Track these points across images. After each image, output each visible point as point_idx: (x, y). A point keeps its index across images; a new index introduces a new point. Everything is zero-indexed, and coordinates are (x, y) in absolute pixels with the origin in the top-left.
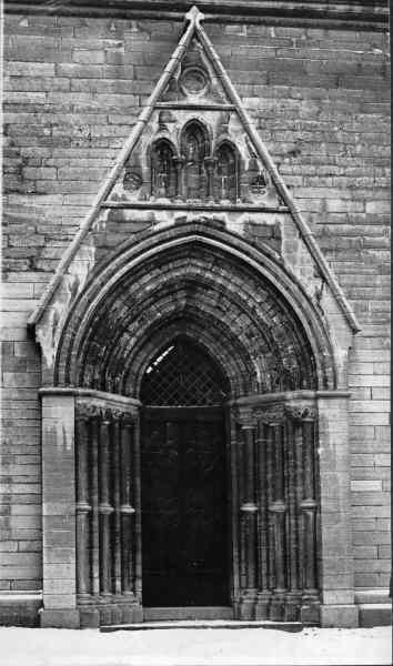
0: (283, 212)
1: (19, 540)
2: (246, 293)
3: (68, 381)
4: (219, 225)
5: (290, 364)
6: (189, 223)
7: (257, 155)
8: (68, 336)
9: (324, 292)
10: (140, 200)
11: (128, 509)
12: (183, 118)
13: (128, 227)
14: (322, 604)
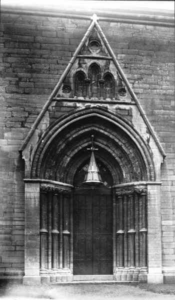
7: (122, 79)
8: (37, 156)
9: (151, 139)
10: (70, 97)
11: (66, 232)
12: (89, 62)
13: (64, 109)
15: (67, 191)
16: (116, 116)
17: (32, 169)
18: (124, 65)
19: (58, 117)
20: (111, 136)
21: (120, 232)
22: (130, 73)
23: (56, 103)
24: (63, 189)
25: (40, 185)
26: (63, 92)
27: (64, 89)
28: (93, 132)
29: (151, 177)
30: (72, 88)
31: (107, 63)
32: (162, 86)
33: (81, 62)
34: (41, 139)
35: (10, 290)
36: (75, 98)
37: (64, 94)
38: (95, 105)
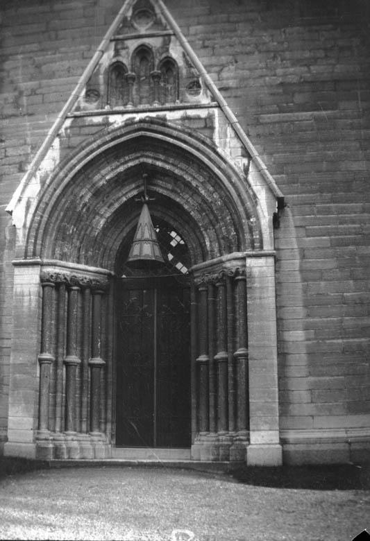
0: (215, 107)
1: (40, 392)
2: (191, 175)
3: (34, 255)
4: (162, 122)
5: (228, 232)
6: (136, 123)
7: (190, 64)
8: (37, 218)
9: (251, 169)
10: (98, 109)
11: (98, 360)
12: (133, 45)
13: (86, 130)
14: (249, 444)
15: (97, 281)
16: (183, 131)
17: (27, 242)
18: (201, 42)
19: (75, 145)
20: (177, 171)
21: (203, 358)
22: (213, 55)
23: (72, 122)
24: (87, 277)
25: (41, 271)
26: (86, 101)
27: (87, 95)
28: (143, 166)
29: (253, 242)
30: (102, 93)
31: (164, 41)
32: (275, 69)
33: (119, 47)
34: (46, 186)
35: (10, 478)
36: (107, 108)
37: (87, 105)
38: (142, 116)
